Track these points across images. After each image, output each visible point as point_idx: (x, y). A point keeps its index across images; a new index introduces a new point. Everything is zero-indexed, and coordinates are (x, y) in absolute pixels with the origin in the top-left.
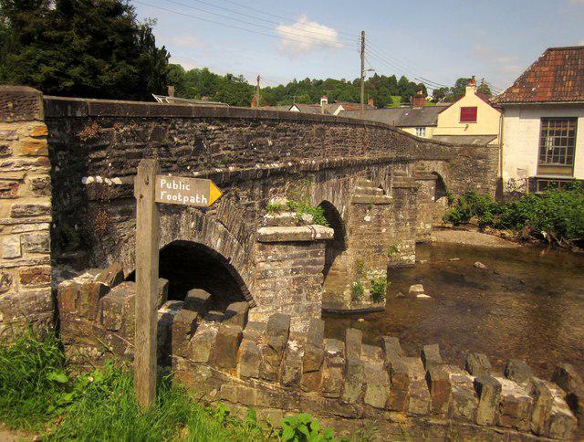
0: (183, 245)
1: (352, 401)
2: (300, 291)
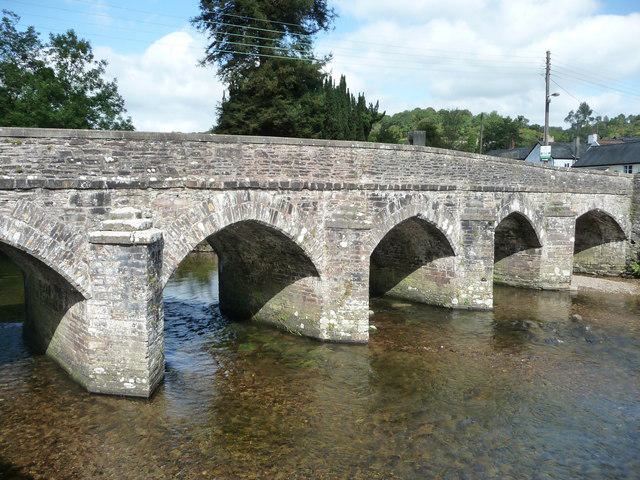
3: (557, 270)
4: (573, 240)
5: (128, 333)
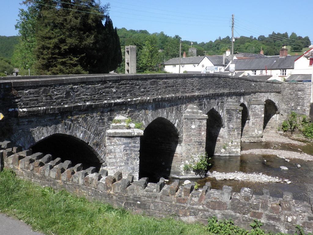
0: (61, 135)
1: (47, 176)
3: (256, 131)
4: (263, 116)
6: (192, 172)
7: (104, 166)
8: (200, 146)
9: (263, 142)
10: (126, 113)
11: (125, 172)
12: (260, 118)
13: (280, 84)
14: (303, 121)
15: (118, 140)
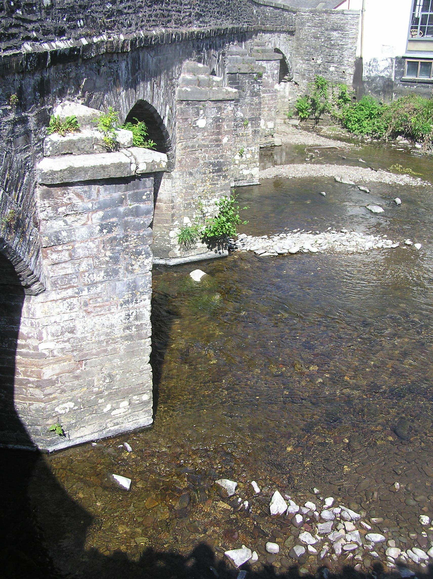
2: (115, 260)
5: (118, 332)
6: (199, 245)
7: (37, 295)
8: (219, 176)
9: (276, 146)
10: (76, 92)
11: (107, 301)
12: (270, 92)
13: (295, 13)
14: (340, 98)
15: (78, 195)
